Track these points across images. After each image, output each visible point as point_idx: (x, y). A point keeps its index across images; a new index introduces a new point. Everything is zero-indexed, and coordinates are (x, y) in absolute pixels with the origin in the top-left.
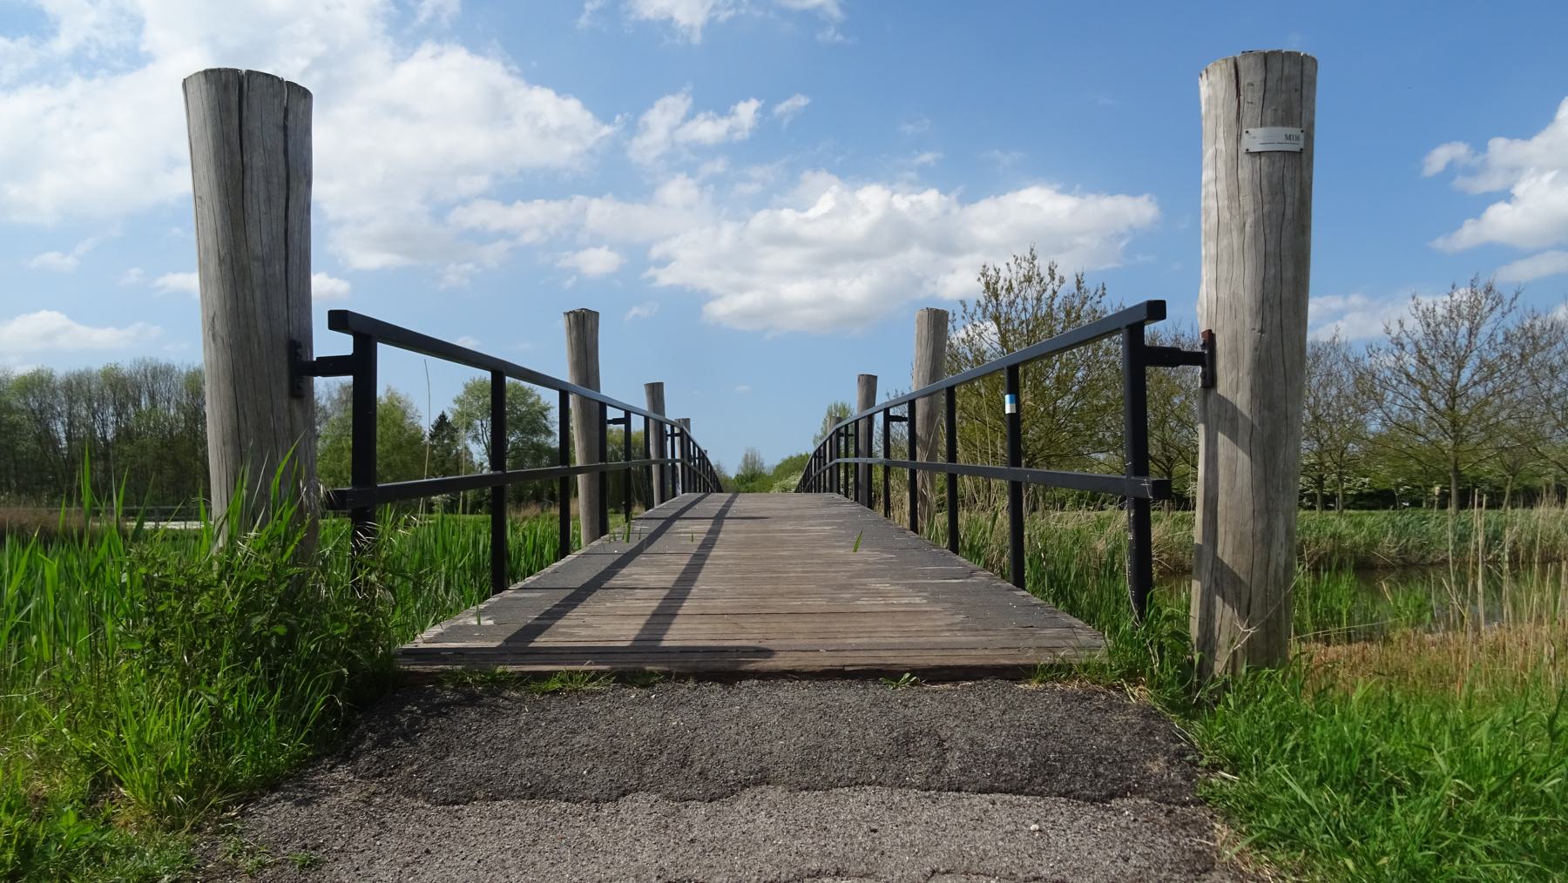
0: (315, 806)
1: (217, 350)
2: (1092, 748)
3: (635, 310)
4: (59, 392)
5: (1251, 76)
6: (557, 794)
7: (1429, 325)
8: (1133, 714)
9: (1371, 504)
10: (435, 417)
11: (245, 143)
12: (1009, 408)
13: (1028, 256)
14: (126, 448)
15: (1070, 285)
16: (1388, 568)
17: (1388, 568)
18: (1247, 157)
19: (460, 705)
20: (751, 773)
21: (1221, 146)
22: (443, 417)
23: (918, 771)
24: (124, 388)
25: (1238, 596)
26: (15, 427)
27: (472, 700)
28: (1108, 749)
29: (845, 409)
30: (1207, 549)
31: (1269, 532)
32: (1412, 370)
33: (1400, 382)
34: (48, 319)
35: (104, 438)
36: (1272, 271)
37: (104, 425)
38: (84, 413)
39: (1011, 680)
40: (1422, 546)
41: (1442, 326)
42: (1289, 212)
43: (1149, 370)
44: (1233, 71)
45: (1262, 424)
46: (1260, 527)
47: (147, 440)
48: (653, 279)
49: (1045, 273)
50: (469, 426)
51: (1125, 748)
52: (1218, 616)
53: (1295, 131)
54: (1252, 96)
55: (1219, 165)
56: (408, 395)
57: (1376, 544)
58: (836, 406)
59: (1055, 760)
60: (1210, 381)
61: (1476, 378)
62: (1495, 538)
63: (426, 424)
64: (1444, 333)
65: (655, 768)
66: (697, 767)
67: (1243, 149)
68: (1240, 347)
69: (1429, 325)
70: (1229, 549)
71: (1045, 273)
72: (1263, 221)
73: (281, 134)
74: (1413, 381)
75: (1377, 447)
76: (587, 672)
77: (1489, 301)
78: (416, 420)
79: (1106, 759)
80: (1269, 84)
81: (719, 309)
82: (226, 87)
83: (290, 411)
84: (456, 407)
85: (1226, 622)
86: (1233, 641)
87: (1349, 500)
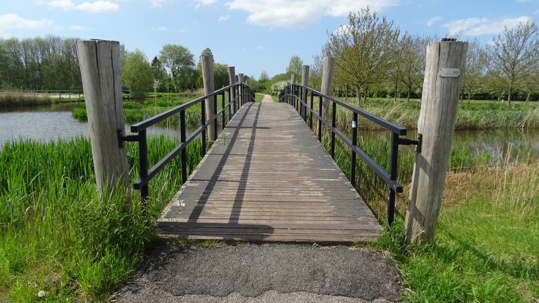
0: (138, 294)
1: (94, 135)
2: (370, 278)
3: (221, 18)
4: (21, 46)
5: (445, 50)
6: (209, 293)
7: (509, 38)
8: (384, 262)
9: (480, 98)
10: (153, 58)
11: (99, 66)
12: (353, 126)
13: (366, 9)
14: (46, 67)
15: (381, 21)
16: (481, 129)
17: (481, 129)
18: (440, 78)
19: (178, 252)
20: (267, 286)
21: (432, 72)
22: (156, 58)
23: (317, 286)
24: (43, 45)
25: (421, 219)
26: (7, 58)
27: (181, 250)
28: (375, 278)
29: (297, 58)
30: (413, 202)
31: (433, 199)
32: (501, 54)
33: (495, 58)
34: (12, 17)
35: (38, 63)
36: (444, 118)
37: (38, 58)
38: (30, 54)
39: (347, 246)
40: (494, 122)
41: (514, 38)
42: (452, 98)
43: (400, 146)
44: (438, 47)
45: (434, 167)
46: (430, 199)
47: (53, 65)
48: (229, 6)
49: (372, 15)
50: (165, 61)
51: (380, 278)
52: (414, 224)
53: (457, 70)
54: (444, 57)
55: (430, 79)
56: (143, 51)
57: (478, 121)
58: (294, 57)
59: (358, 283)
60: (419, 150)
61: (523, 58)
62: (520, 119)
63: (150, 61)
64: (514, 41)
65: (238, 282)
66: (251, 283)
67: (439, 75)
68: (430, 142)
69: (509, 38)
70: (419, 205)
71: (372, 15)
72: (442, 100)
73: (111, 61)
74: (501, 58)
75: (484, 80)
76: (217, 240)
77: (533, 29)
78: (147, 60)
79: (374, 283)
80: (450, 53)
81: (252, 19)
82: (91, 47)
83: (119, 153)
84: (160, 54)
85: (416, 226)
86: (418, 232)
87: (473, 96)
